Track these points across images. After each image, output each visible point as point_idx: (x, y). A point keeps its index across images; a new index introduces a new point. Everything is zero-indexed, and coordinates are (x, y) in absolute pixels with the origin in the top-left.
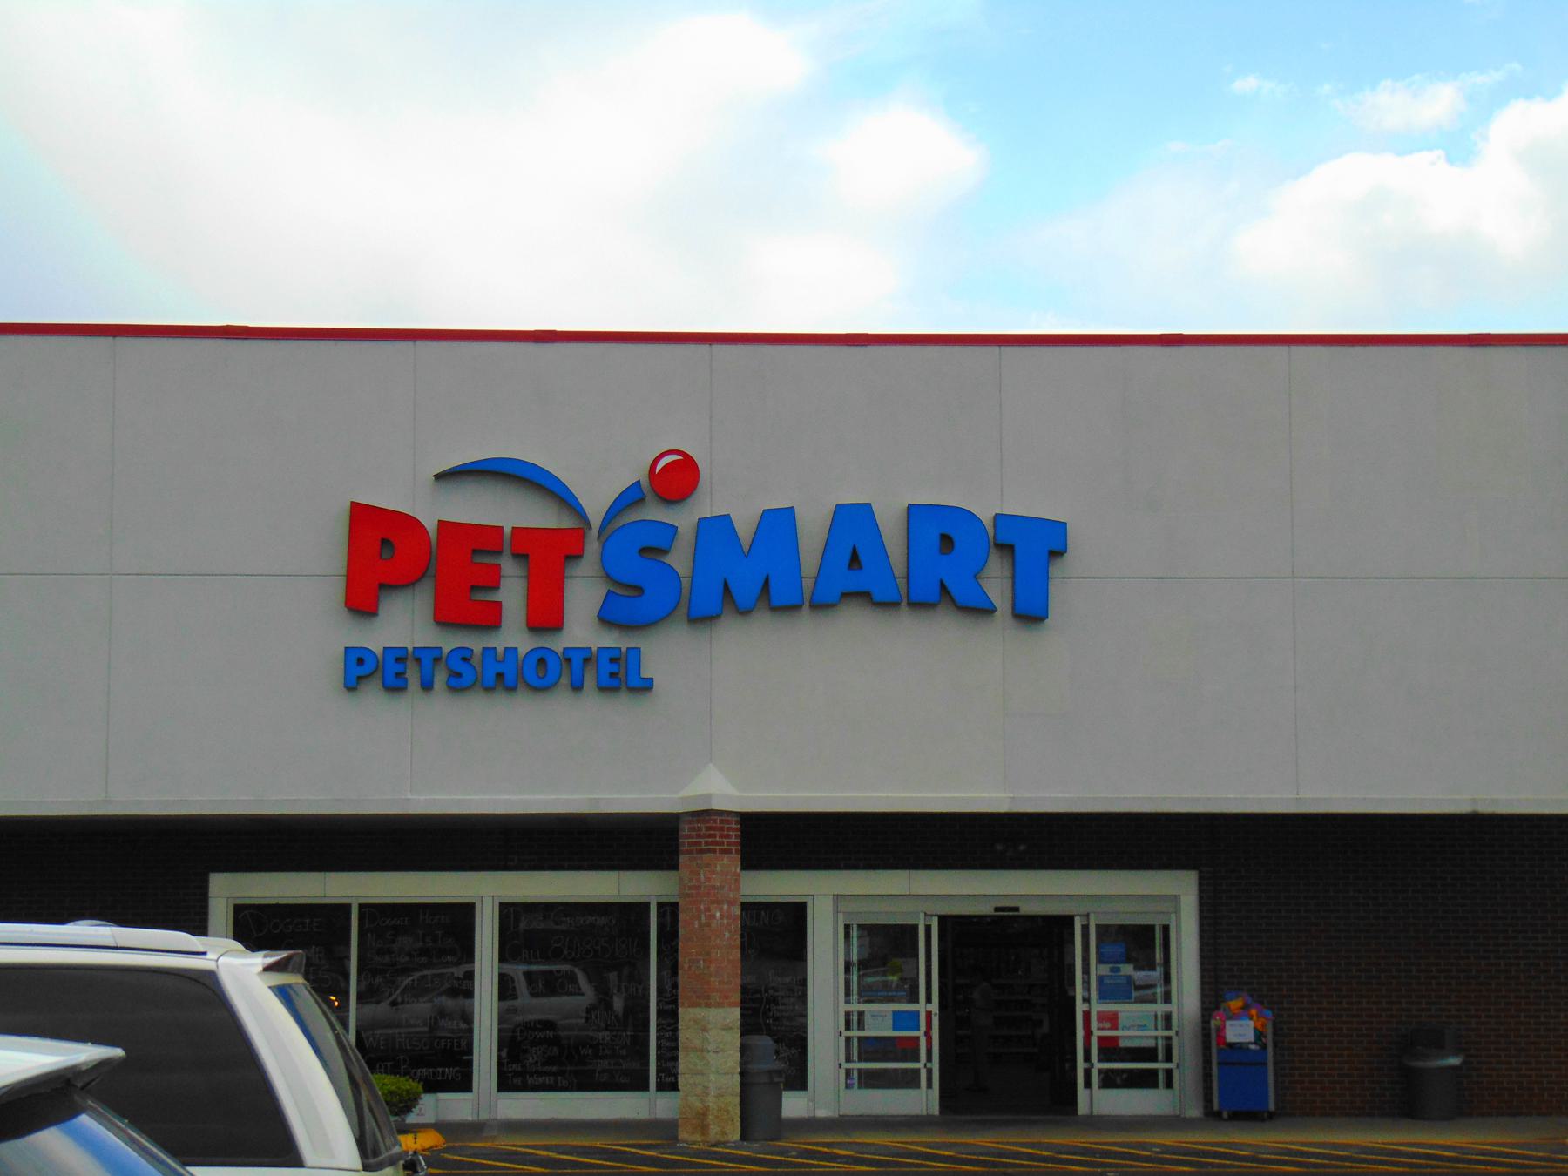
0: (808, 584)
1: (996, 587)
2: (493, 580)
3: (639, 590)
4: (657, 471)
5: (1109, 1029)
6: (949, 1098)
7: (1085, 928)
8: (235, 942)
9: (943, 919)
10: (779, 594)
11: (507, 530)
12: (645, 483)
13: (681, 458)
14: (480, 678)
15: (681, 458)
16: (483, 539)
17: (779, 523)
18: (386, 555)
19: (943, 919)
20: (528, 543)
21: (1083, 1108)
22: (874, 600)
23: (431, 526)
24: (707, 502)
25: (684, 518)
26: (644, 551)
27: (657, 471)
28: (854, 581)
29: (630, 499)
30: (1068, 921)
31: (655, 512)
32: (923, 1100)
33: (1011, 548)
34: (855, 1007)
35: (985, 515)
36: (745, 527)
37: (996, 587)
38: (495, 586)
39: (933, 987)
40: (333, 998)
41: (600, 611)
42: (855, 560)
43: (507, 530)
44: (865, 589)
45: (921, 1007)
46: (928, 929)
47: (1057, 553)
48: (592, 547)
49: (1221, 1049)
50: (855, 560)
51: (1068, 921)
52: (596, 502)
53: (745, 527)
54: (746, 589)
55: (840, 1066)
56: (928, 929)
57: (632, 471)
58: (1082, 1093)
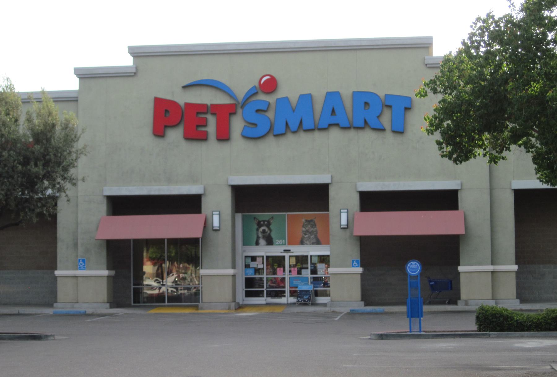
2: (204, 123)
3: (255, 125)
5: (311, 281)
8: (127, 49)
10: (305, 125)
13: (554, 169)
16: (201, 109)
18: (168, 115)
20: (215, 109)
24: (281, 93)
25: (271, 99)
26: (258, 111)
28: (333, 120)
29: (252, 94)
31: (262, 97)
37: (386, 120)
38: (205, 126)
40: (534, 49)
41: (243, 130)
42: (333, 112)
44: (336, 122)
47: (407, 109)
49: (432, 285)
50: (333, 112)
52: (241, 94)
54: (294, 125)
55: (243, 290)
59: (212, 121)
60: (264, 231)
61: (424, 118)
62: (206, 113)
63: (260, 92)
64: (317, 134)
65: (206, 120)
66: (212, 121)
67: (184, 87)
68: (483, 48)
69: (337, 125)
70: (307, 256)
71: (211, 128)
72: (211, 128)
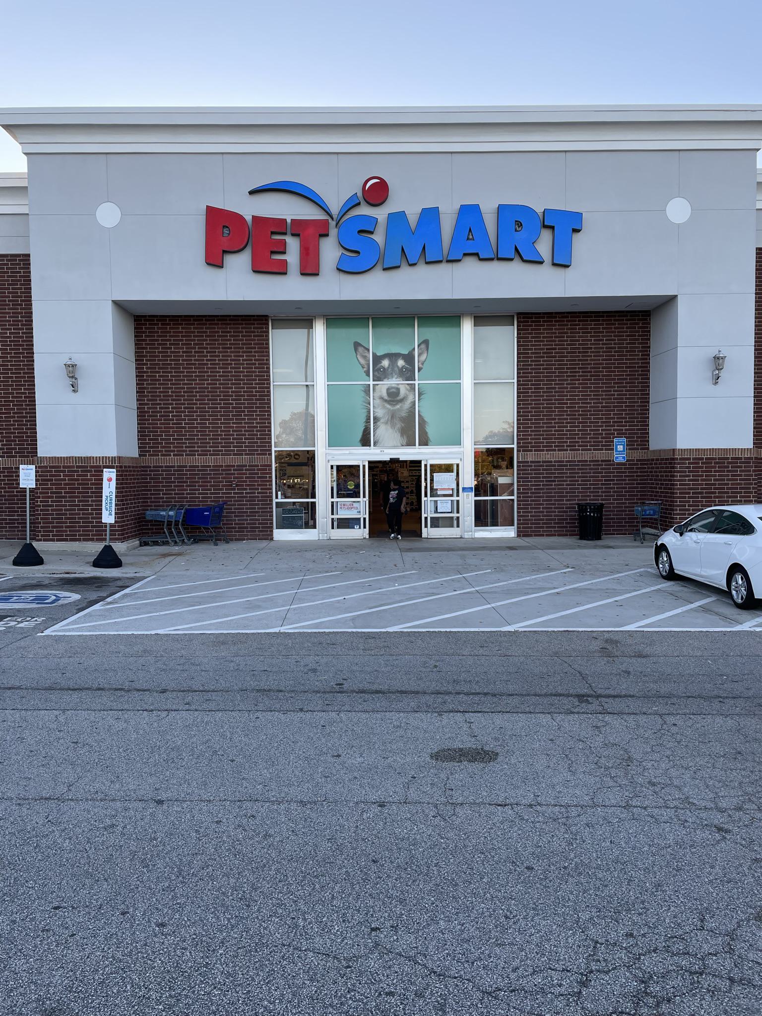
0: (445, 251)
1: (544, 246)
4: (367, 188)
6: (372, 534)
7: (426, 466)
9: (370, 462)
11: (289, 221)
12: (360, 194)
13: (379, 181)
14: (381, 257)
15: (379, 181)
16: (278, 226)
17: (430, 215)
19: (370, 462)
20: (299, 228)
21: (424, 535)
22: (481, 257)
23: (249, 219)
25: (381, 214)
26: (360, 232)
27: (367, 188)
30: (420, 462)
31: (365, 210)
32: (361, 533)
33: (552, 228)
34: (335, 500)
35: (539, 210)
36: (413, 220)
37: (544, 246)
39: (455, 460)
43: (289, 221)
45: (361, 499)
46: (364, 466)
48: (333, 232)
51: (420, 462)
53: (413, 220)
56: (364, 466)
57: (353, 187)
58: (424, 530)
59: (293, 245)
60: (393, 396)
61: (758, 656)
62: (285, 234)
63: (363, 202)
64: (444, 267)
65: (284, 243)
66: (293, 245)
67: (252, 193)
68: (487, 433)
69: (477, 255)
70: (338, 528)
71: (293, 254)
72: (293, 254)
